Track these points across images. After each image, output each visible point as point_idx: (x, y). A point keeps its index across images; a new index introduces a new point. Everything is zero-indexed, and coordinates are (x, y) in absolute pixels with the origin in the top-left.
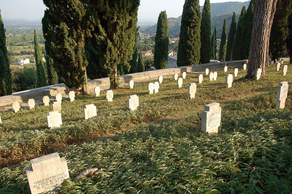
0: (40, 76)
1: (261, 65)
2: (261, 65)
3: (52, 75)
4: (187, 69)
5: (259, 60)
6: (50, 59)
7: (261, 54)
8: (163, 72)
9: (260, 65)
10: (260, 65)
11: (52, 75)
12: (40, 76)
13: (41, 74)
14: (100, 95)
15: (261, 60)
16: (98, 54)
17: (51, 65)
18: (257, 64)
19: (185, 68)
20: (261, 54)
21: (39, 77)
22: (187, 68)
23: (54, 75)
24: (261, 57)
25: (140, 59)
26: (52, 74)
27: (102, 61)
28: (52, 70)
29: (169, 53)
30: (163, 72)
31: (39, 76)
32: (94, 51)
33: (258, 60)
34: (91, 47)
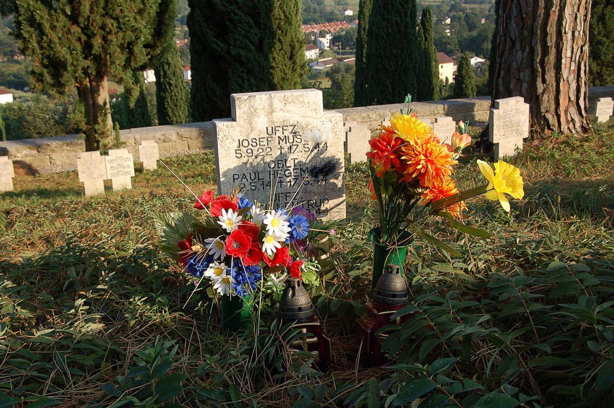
0: (133, 116)
1: (544, 81)
2: (544, 81)
3: (169, 115)
4: (475, 109)
5: (532, 51)
6: (163, 68)
7: (540, 21)
8: (364, 115)
9: (539, 80)
10: (539, 80)
11: (170, 118)
12: (133, 116)
13: (137, 113)
14: (15, 188)
15: (545, 52)
16: (224, 50)
17: (166, 87)
18: (522, 75)
19: (465, 104)
20: (540, 21)
21: (129, 119)
22: (473, 105)
23: (176, 116)
24: (545, 34)
25: (463, 78)
26: (171, 114)
27: (239, 77)
28: (168, 102)
29: (186, 18)
30: (364, 115)
31: (131, 117)
32: (214, 42)
33: (525, 54)
34: (203, 29)
